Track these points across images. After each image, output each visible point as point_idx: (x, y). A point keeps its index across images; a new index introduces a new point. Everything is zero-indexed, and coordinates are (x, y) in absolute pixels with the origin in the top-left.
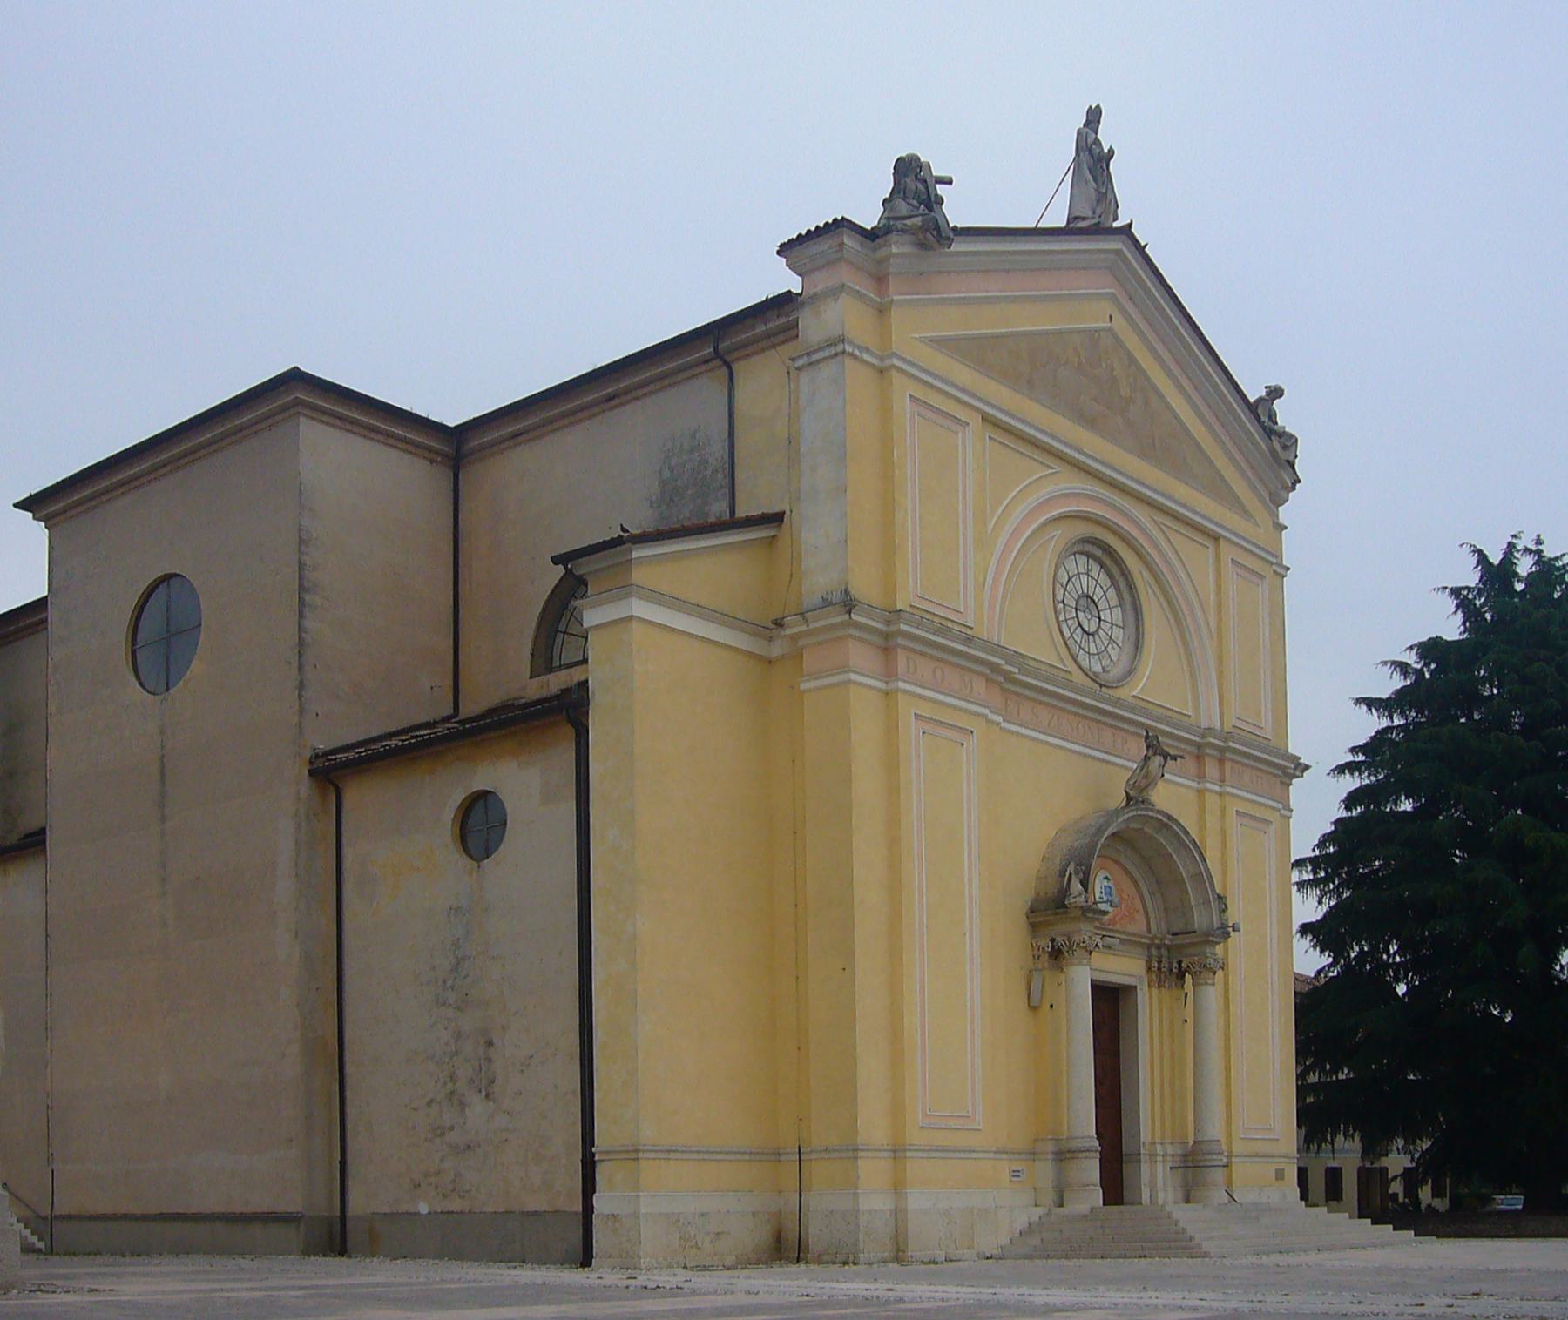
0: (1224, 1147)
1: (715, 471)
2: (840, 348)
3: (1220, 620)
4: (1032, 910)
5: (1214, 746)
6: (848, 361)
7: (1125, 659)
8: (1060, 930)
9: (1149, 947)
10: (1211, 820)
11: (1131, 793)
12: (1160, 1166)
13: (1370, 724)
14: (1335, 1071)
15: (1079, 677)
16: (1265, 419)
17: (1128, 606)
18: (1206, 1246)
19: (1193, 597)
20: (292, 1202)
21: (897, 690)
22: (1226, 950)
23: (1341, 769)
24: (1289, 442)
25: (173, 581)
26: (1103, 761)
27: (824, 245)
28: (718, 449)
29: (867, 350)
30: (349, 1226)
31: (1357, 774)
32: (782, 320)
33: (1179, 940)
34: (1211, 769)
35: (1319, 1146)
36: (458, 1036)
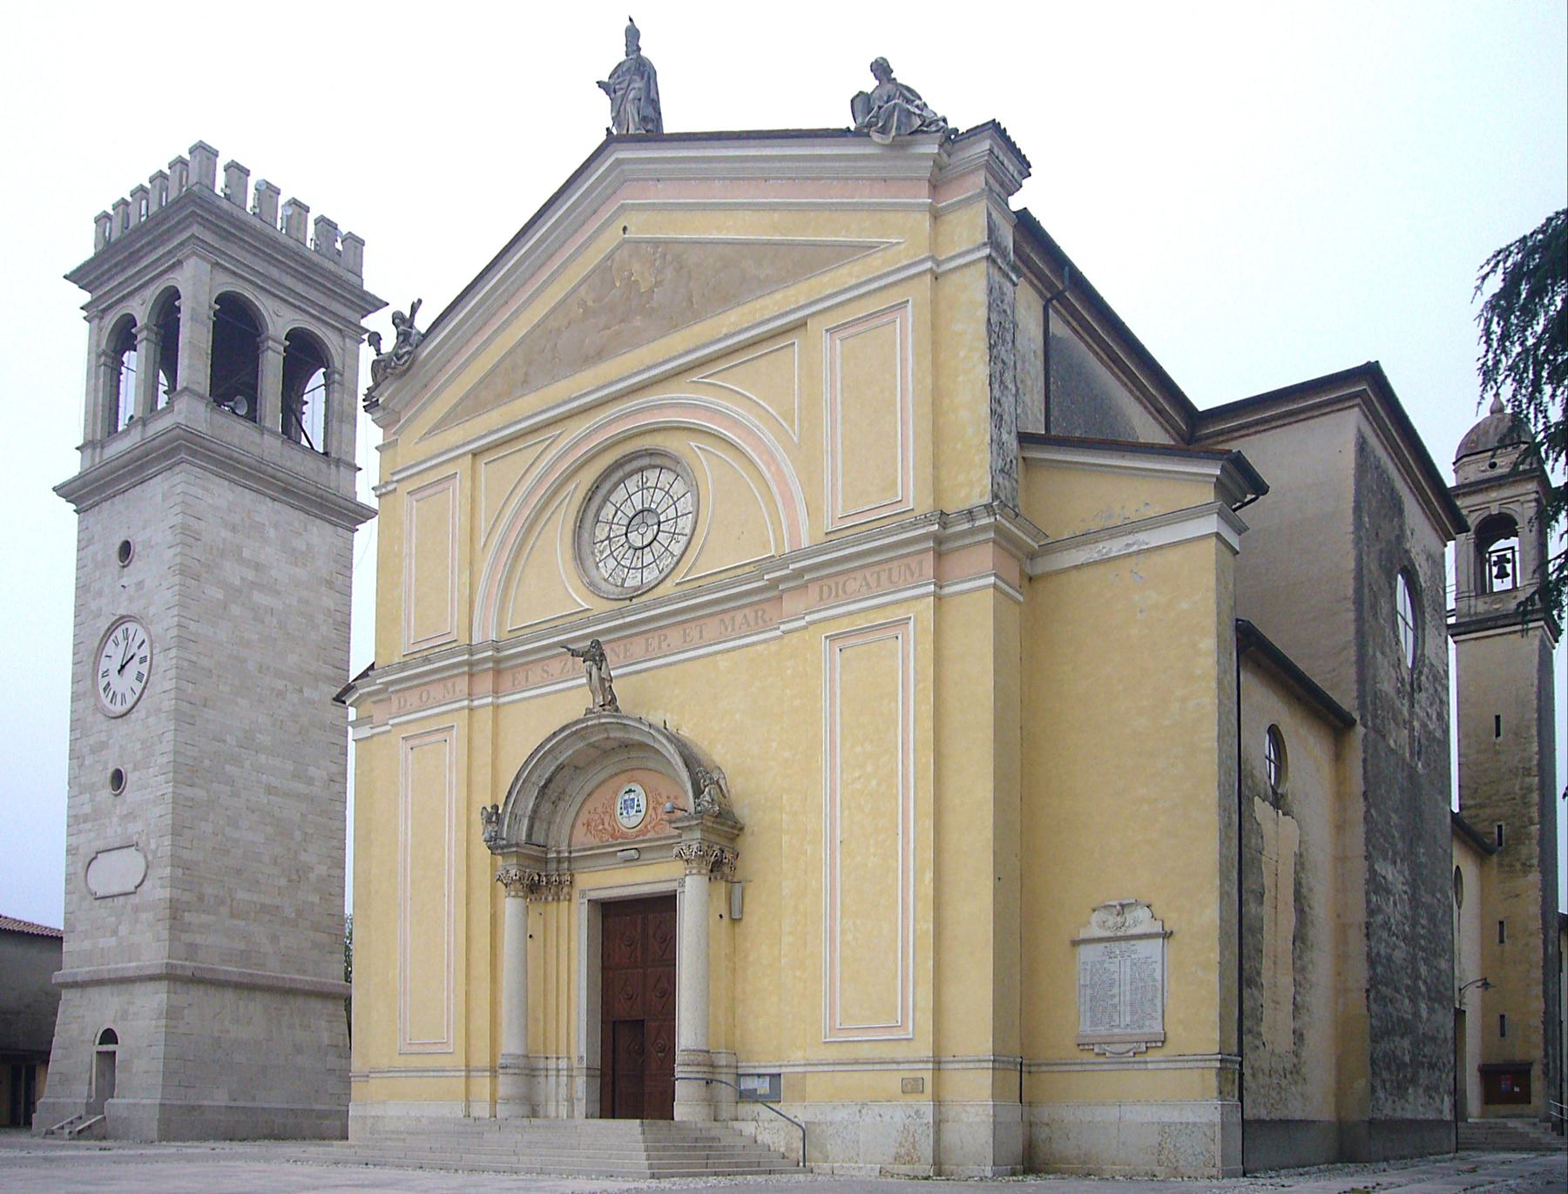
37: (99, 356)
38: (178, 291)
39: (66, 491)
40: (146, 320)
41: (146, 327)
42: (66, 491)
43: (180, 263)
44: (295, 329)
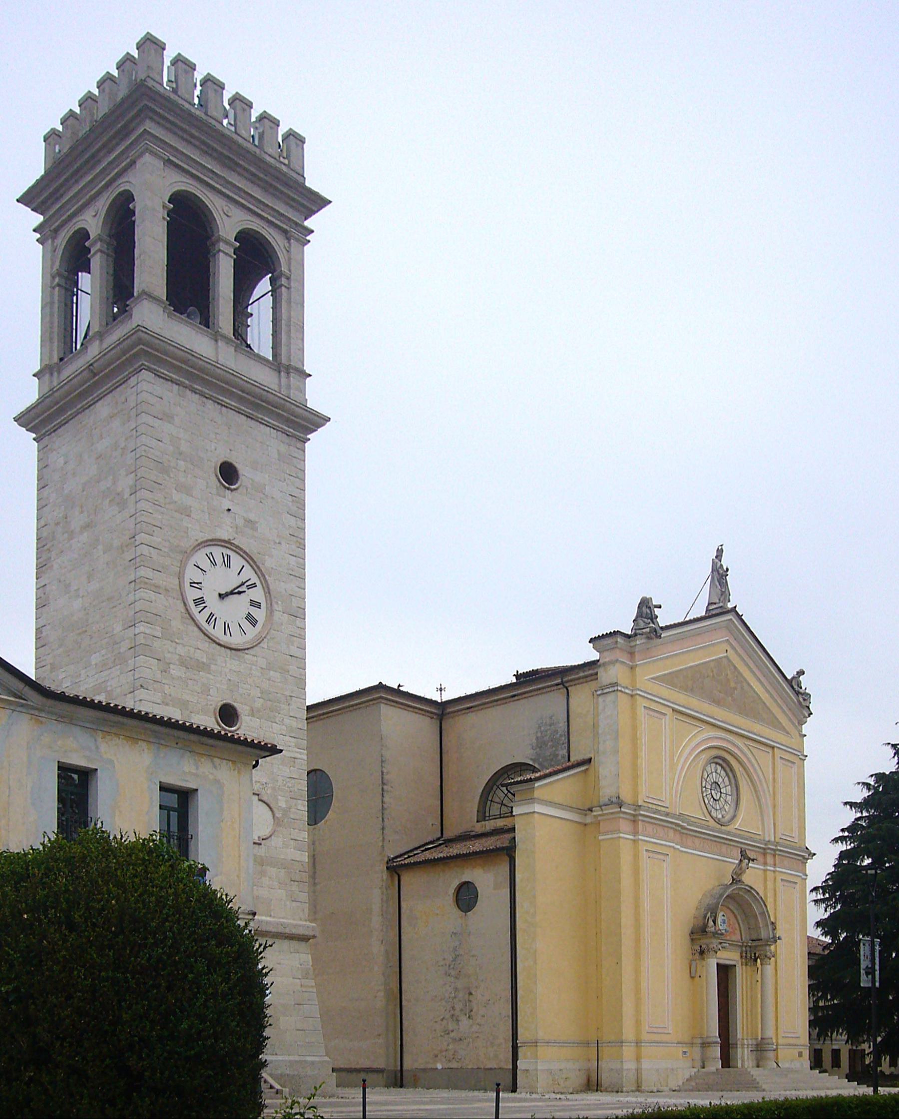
0: (774, 1041)
1: (561, 736)
2: (616, 688)
3: (774, 787)
4: (692, 933)
5: (772, 849)
6: (619, 693)
7: (732, 811)
8: (704, 942)
9: (741, 946)
10: (770, 885)
11: (735, 877)
12: (746, 1050)
13: (851, 816)
14: (832, 999)
15: (712, 823)
16: (796, 687)
17: (733, 785)
18: (764, 1087)
19: (762, 777)
20: (380, 1064)
21: (639, 839)
22: (776, 948)
23: (836, 840)
24: (807, 696)
25: (318, 772)
26: (723, 861)
27: (609, 641)
28: (562, 725)
29: (627, 688)
30: (404, 1074)
31: (844, 842)
32: (591, 672)
33: (755, 944)
34: (770, 859)
35: (825, 1039)
36: (456, 989)
37: (53, 277)
38: (133, 195)
39: (26, 419)
40: (99, 232)
41: (99, 238)
42: (26, 419)
43: (133, 163)
44: (244, 229)
